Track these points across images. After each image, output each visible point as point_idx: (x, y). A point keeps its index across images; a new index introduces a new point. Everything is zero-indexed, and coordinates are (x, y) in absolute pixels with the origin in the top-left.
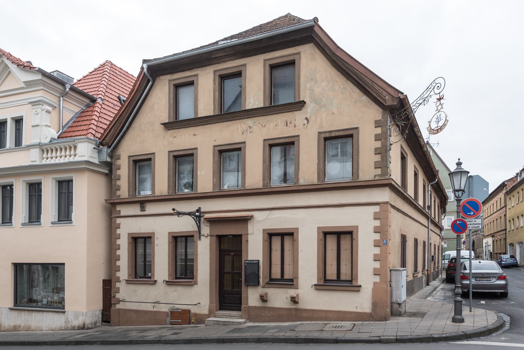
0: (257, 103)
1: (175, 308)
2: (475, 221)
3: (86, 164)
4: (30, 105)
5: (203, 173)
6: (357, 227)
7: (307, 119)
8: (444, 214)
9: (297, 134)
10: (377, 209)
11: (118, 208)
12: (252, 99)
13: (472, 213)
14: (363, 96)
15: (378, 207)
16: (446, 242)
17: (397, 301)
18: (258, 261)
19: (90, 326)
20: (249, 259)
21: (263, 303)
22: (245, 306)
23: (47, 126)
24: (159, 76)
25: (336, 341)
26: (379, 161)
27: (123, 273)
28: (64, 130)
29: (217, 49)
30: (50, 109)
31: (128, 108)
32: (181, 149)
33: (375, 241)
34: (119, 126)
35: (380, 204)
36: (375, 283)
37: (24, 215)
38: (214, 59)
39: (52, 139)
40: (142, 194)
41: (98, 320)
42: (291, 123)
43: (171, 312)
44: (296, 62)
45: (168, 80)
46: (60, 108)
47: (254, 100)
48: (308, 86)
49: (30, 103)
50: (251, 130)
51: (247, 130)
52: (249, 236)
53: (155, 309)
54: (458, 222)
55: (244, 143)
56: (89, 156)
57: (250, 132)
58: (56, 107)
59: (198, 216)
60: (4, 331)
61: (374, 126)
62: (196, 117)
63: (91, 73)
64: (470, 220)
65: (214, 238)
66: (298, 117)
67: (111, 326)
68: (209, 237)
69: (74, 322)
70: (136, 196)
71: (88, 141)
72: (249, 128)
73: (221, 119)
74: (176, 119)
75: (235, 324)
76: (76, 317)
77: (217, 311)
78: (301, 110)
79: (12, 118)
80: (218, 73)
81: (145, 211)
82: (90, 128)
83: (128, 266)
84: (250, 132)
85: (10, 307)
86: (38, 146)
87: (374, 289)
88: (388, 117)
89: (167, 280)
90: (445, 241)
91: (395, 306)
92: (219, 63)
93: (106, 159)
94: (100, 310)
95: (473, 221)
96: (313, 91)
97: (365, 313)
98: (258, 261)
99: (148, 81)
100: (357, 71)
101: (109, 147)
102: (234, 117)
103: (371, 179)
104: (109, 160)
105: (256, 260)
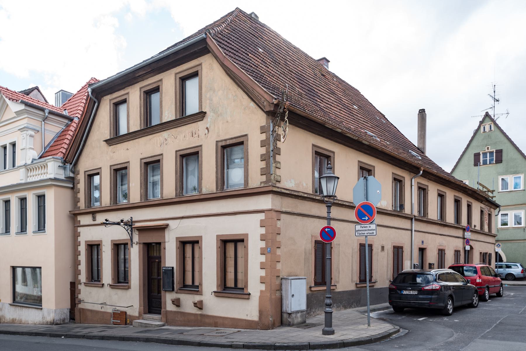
0: (170, 116)
1: (116, 310)
2: (370, 227)
3: (51, 181)
4: (19, 131)
5: (133, 184)
6: (247, 235)
7: (207, 128)
8: (498, 208)
9: (200, 144)
10: (262, 216)
11: (79, 218)
12: (167, 112)
13: (367, 218)
14: (251, 103)
15: (263, 214)
16: (500, 246)
17: (286, 311)
18: (173, 268)
19: (59, 322)
20: (167, 266)
21: (177, 308)
22: (164, 310)
23: (30, 148)
24: (103, 97)
25: (200, 344)
26: (264, 168)
27: (83, 277)
28: (46, 150)
29: (143, 66)
30: (32, 133)
31: (81, 129)
32: (118, 163)
33: (261, 248)
34: (76, 146)
35: (265, 212)
36: (261, 292)
37: (34, 225)
38: (138, 77)
39: (34, 160)
40: (95, 206)
41: (66, 318)
42: (195, 133)
43: (114, 313)
44: (199, 74)
45: (109, 100)
46: (42, 131)
47: (168, 113)
48: (208, 96)
49: (19, 130)
50: (166, 143)
51: (164, 143)
52: (166, 243)
53: (103, 310)
54: (326, 230)
55: (162, 154)
56: (56, 173)
57: (166, 144)
58: (38, 131)
59: (129, 224)
60: (7, 323)
61: (260, 132)
62: (128, 133)
63: (78, 92)
64: (365, 226)
65: (142, 245)
66: (200, 126)
67: (75, 323)
68: (138, 244)
69: (47, 318)
70: (117, 204)
71: (54, 161)
72: (165, 141)
73: (144, 134)
74: (116, 135)
75: (153, 326)
76: (49, 314)
77: (145, 313)
78: (202, 120)
79: (10, 143)
80: (143, 90)
81: (96, 220)
82: (62, 147)
83: (86, 271)
84: (166, 144)
85: (10, 303)
86: (24, 167)
87: (260, 297)
88: (271, 122)
89: (111, 284)
90: (498, 244)
91: (285, 316)
92: (143, 80)
93: (69, 174)
94: (68, 309)
95: (368, 227)
96: (212, 101)
97: (253, 321)
98: (173, 268)
99: (95, 102)
100: (240, 79)
101: (71, 164)
102: (154, 131)
103: (258, 187)
104: (72, 175)
105: (170, 267)
